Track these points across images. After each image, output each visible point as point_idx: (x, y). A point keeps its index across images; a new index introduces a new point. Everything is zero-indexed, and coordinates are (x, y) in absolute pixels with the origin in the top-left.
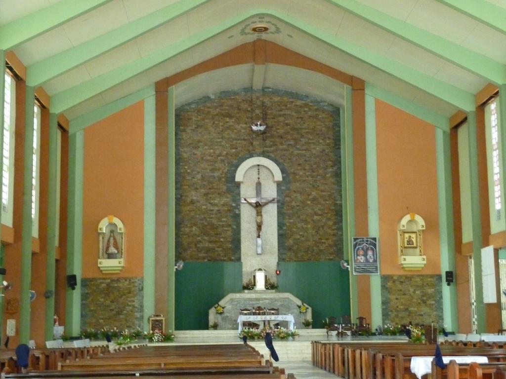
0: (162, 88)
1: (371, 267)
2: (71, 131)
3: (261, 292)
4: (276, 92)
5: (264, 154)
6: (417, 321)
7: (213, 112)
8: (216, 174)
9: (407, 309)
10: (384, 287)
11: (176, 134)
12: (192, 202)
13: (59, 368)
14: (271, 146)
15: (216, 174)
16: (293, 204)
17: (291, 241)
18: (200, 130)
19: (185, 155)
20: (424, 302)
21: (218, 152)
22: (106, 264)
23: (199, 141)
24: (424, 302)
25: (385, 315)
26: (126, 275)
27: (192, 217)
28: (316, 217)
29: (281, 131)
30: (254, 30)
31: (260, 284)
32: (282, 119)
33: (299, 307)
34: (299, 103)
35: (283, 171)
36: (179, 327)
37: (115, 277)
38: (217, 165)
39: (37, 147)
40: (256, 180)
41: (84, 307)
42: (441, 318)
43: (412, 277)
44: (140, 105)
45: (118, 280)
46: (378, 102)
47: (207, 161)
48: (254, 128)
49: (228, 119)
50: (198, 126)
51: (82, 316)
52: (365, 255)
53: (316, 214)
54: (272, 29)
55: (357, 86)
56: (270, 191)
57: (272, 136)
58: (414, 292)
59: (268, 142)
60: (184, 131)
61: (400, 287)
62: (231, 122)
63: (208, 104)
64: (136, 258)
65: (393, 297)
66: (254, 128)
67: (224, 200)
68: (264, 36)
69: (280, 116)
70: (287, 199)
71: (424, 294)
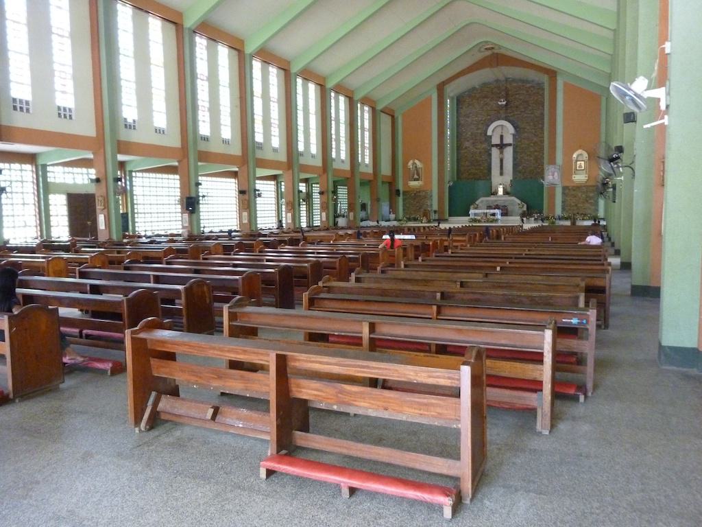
0: (441, 88)
1: (160, 207)
2: (396, 116)
3: (501, 196)
4: (514, 80)
5: (506, 119)
6: (581, 212)
7: (478, 95)
8: (479, 131)
9: (576, 205)
10: (563, 193)
11: (457, 110)
12: (466, 148)
13: (503, 238)
14: (510, 113)
15: (479, 131)
16: (523, 146)
17: (520, 167)
18: (470, 107)
19: (462, 122)
20: (587, 201)
21: (480, 119)
22: (413, 184)
23: (470, 113)
24: (587, 201)
25: (563, 209)
26: (425, 189)
27: (466, 156)
28: (536, 153)
29: (517, 103)
30: (486, 49)
31: (501, 191)
32: (517, 96)
33: (519, 204)
34: (528, 85)
35: (515, 128)
36: (450, 215)
37: (418, 190)
38: (480, 126)
39: (369, 126)
40: (500, 134)
41: (404, 205)
42: (597, 210)
43: (581, 187)
44: (429, 99)
45: (419, 192)
46: (566, 84)
47: (474, 124)
48: (500, 103)
49: (486, 100)
50: (469, 105)
51: (404, 210)
52: (553, 175)
53: (536, 151)
54: (497, 47)
55: (552, 74)
56: (509, 139)
57: (511, 107)
58: (581, 195)
59: (509, 111)
60: (461, 108)
61: (573, 193)
62: (488, 100)
63: (475, 91)
64: (428, 181)
65: (568, 199)
66: (500, 103)
67: (484, 146)
68: (496, 51)
69: (516, 94)
70: (519, 143)
71: (587, 197)
